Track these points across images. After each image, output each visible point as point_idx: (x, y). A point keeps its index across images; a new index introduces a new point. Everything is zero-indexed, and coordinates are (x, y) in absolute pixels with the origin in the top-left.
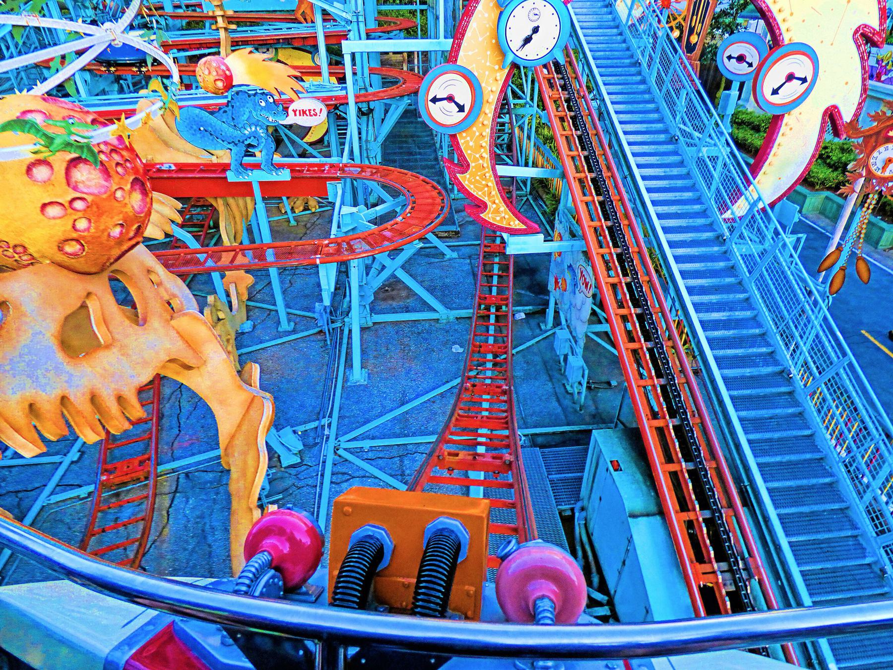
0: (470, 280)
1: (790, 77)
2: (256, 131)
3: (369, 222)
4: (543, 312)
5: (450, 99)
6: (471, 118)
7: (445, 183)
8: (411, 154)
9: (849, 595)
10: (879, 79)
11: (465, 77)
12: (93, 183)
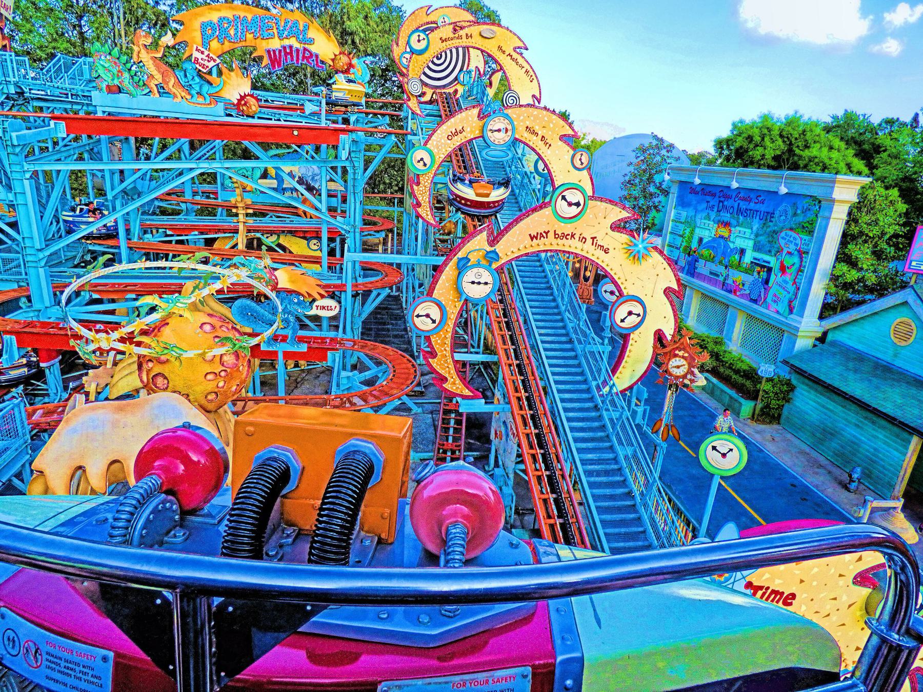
0: (432, 430)
1: (630, 313)
2: (287, 318)
3: (361, 383)
4: (486, 457)
5: (428, 316)
6: (440, 327)
7: (412, 351)
8: (384, 324)
9: (614, 583)
10: (735, 294)
11: (437, 305)
12: (230, 362)
